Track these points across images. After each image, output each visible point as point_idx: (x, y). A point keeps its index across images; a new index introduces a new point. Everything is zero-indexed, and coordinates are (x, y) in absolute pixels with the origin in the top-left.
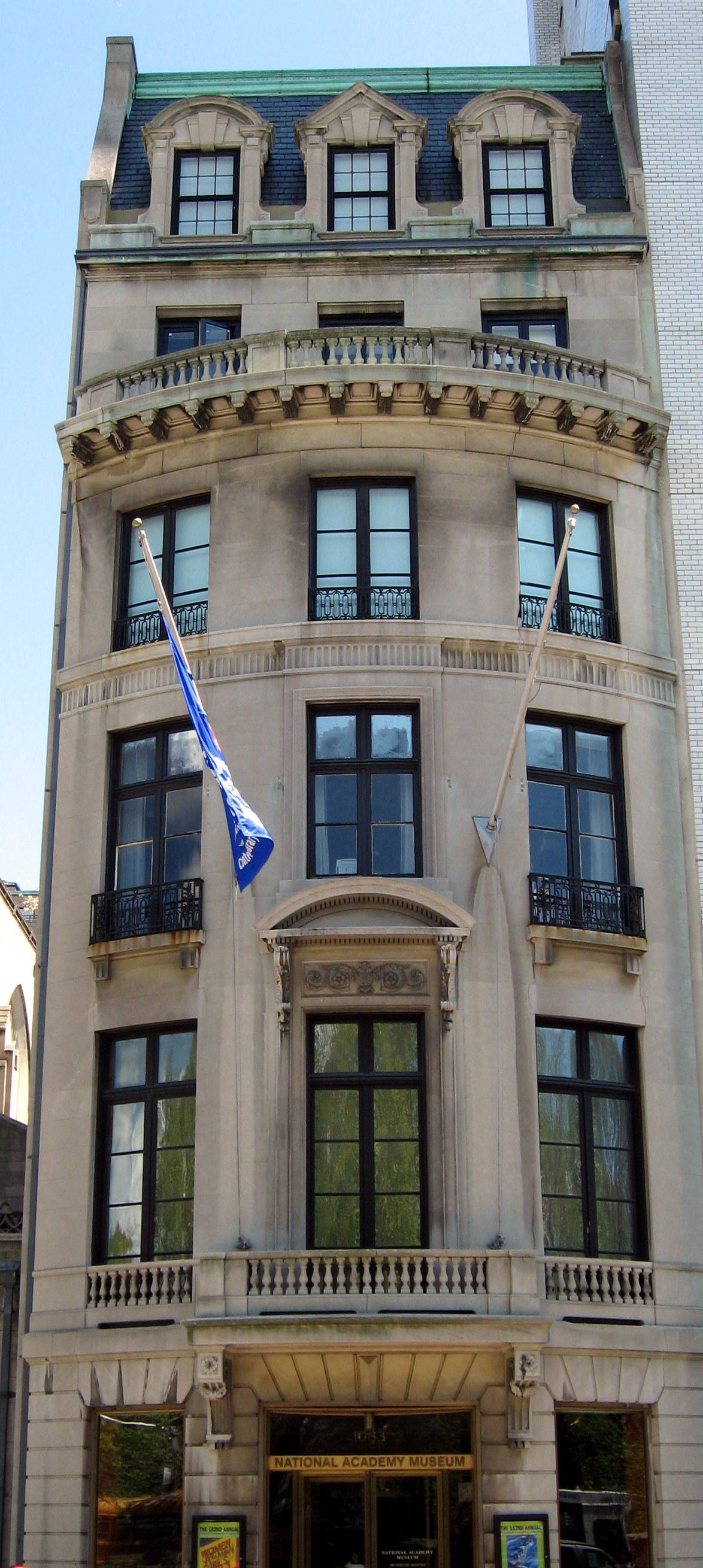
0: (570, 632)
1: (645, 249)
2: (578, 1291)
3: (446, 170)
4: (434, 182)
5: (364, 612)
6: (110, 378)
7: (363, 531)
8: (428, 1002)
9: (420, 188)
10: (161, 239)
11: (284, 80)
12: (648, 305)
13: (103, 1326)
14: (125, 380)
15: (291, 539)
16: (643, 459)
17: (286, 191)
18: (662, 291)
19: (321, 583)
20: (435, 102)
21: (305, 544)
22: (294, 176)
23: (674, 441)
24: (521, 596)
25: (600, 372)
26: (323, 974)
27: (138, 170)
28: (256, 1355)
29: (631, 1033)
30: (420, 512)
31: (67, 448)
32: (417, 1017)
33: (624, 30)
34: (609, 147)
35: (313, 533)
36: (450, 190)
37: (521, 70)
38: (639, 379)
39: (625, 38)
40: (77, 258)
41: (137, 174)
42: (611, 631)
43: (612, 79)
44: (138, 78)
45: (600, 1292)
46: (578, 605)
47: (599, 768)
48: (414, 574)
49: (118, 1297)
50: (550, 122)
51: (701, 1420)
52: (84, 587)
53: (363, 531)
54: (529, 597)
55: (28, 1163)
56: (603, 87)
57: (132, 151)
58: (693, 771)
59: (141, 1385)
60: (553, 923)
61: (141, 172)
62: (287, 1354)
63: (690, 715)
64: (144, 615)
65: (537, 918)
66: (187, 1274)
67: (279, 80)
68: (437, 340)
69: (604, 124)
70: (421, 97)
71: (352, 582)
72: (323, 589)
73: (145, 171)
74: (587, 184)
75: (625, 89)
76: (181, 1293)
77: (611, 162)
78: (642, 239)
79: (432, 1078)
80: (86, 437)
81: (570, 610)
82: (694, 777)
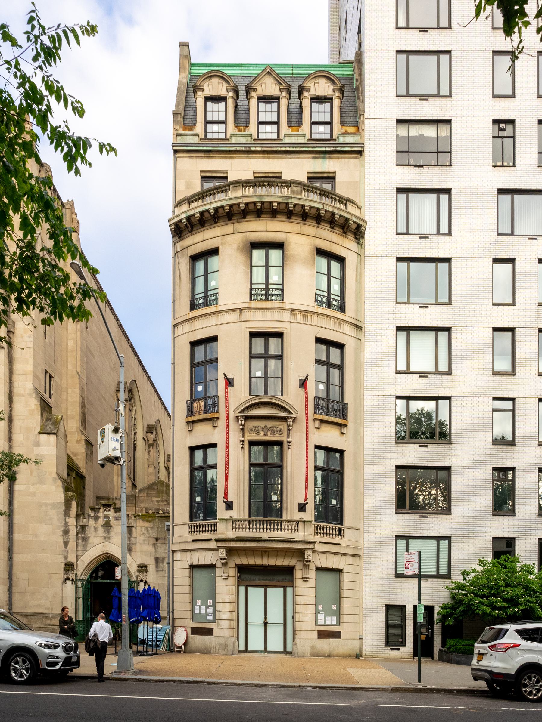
0: (330, 309)
1: (363, 149)
2: (323, 534)
3: (297, 112)
4: (293, 118)
5: (267, 299)
6: (184, 200)
7: (267, 266)
8: (284, 439)
9: (289, 120)
10: (201, 139)
11: (242, 68)
12: (362, 174)
13: (193, 541)
14: (190, 200)
15: (244, 268)
16: (357, 241)
17: (243, 120)
18: (368, 169)
19: (254, 286)
20: (294, 80)
21: (249, 271)
22: (246, 113)
23: (368, 234)
24: (316, 294)
25: (345, 201)
26: (254, 429)
27: (192, 108)
28: (235, 550)
29: (341, 452)
30: (285, 259)
31: (172, 229)
32: (279, 444)
33: (362, 44)
34: (353, 103)
35: (251, 266)
36: (299, 121)
37: (325, 66)
38: (358, 207)
39: (362, 49)
40: (173, 146)
41: (192, 110)
42: (342, 309)
43: (357, 71)
44: (192, 65)
45: (329, 534)
46: (333, 299)
47: (337, 362)
48: (283, 284)
49: (197, 531)
50: (334, 621)
51: (452, 1)
52: (180, 288)
53: (267, 266)
54: (318, 295)
55: (171, 490)
56: (353, 75)
57: (190, 99)
58: (365, 363)
59: (204, 558)
60: (321, 414)
61: (193, 109)
62: (243, 550)
63: (365, 343)
64: (199, 298)
65: (316, 412)
66: (215, 525)
67: (240, 68)
68: (292, 185)
69: (352, 93)
70: (289, 78)
71: (263, 286)
72: (254, 289)
73: (195, 109)
74: (345, 120)
75: (361, 74)
76: (214, 531)
77: (354, 110)
78: (362, 145)
79: (285, 465)
80: (178, 225)
81: (330, 300)
82: (365, 365)
